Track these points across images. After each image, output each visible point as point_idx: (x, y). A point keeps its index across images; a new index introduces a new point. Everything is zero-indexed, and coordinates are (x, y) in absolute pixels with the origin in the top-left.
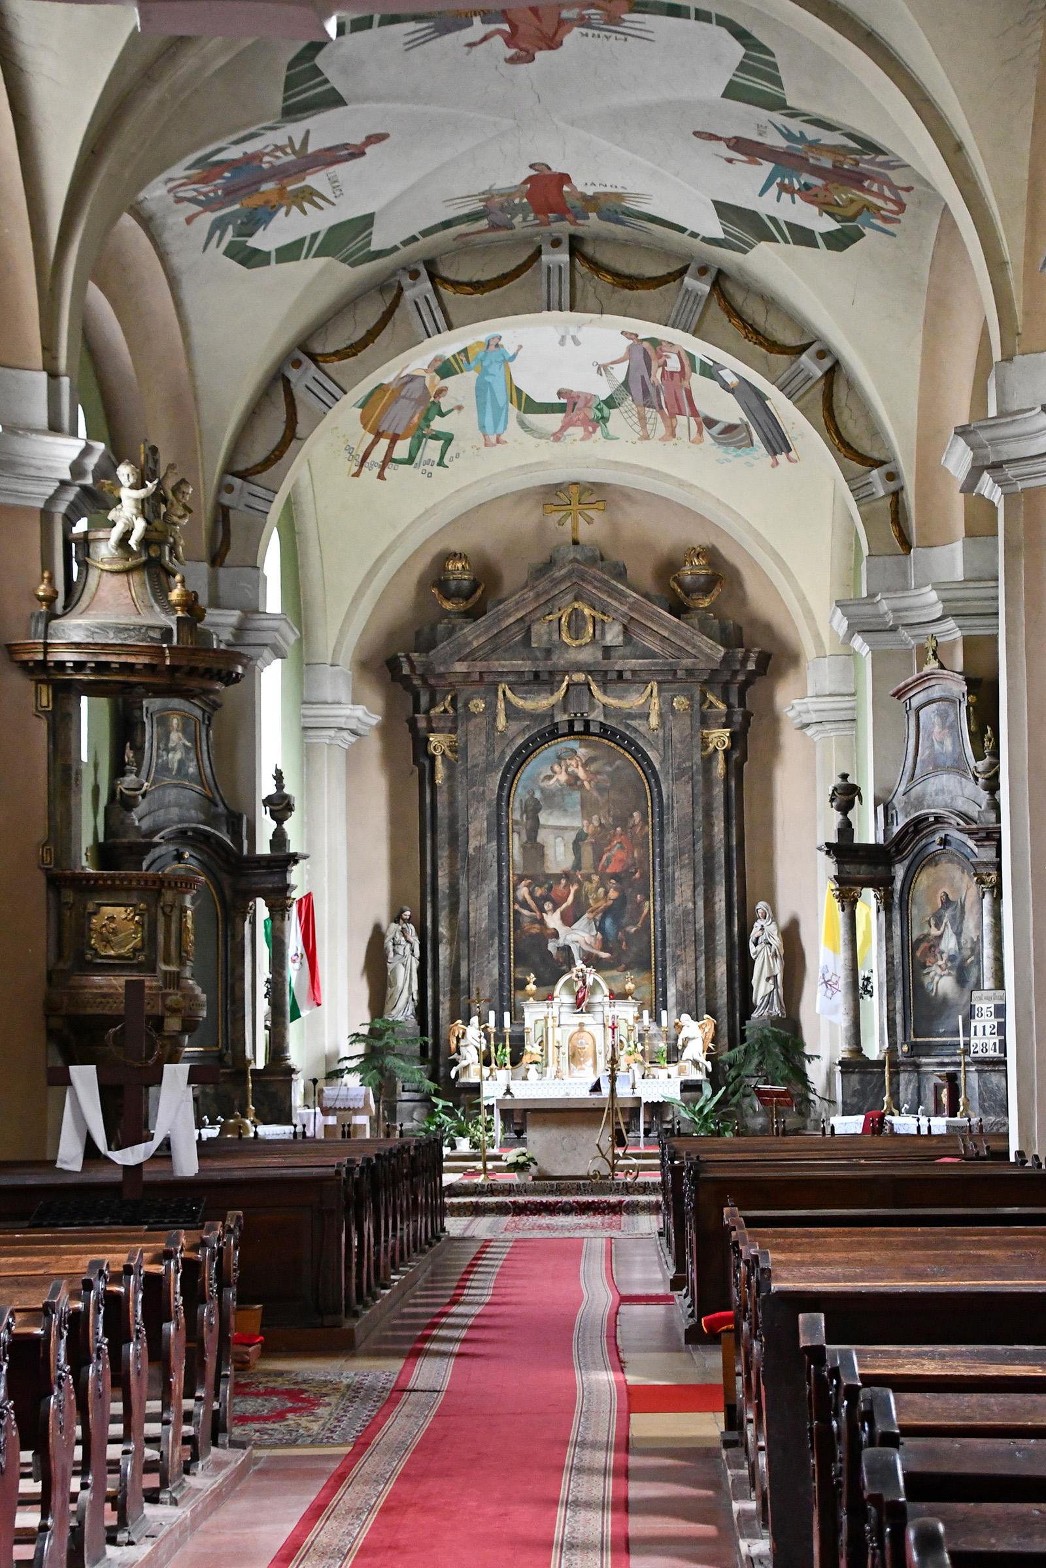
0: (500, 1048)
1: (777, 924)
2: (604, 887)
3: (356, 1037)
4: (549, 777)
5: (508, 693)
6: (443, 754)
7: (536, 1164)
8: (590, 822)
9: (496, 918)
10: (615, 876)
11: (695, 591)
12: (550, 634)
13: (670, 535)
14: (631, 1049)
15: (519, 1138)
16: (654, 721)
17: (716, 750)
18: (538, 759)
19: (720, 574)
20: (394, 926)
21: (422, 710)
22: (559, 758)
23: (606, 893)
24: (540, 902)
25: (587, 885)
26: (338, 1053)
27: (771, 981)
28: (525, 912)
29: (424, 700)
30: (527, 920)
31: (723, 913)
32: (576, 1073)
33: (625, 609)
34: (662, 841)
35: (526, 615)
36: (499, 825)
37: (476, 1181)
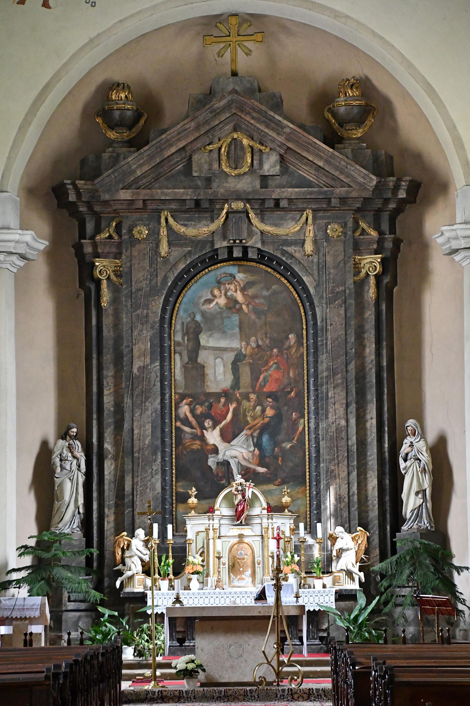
0: (163, 559)
1: (426, 441)
2: (262, 405)
3: (24, 550)
4: (210, 301)
5: (171, 220)
6: (108, 278)
7: (204, 670)
8: (248, 344)
9: (159, 435)
10: (270, 395)
11: (349, 122)
12: (211, 164)
13: (326, 66)
14: (288, 560)
15: (181, 645)
16: (309, 247)
17: (367, 275)
18: (199, 283)
19: (372, 104)
20: (61, 442)
21: (88, 236)
22: (219, 282)
23: (263, 411)
24: (200, 419)
25: (245, 404)
26: (6, 565)
27: (420, 496)
28: (187, 429)
29: (90, 227)
30: (188, 436)
31: (374, 430)
32: (236, 583)
33: (281, 139)
34: (316, 362)
35: (187, 145)
36: (162, 346)
37: (146, 687)
